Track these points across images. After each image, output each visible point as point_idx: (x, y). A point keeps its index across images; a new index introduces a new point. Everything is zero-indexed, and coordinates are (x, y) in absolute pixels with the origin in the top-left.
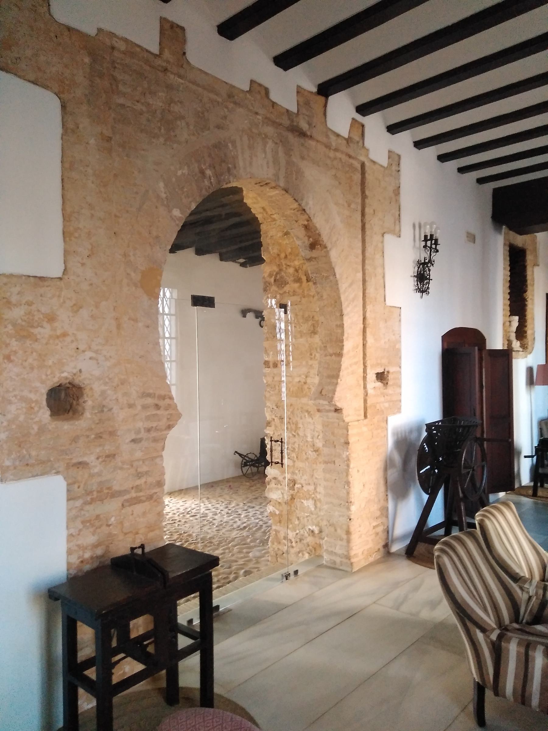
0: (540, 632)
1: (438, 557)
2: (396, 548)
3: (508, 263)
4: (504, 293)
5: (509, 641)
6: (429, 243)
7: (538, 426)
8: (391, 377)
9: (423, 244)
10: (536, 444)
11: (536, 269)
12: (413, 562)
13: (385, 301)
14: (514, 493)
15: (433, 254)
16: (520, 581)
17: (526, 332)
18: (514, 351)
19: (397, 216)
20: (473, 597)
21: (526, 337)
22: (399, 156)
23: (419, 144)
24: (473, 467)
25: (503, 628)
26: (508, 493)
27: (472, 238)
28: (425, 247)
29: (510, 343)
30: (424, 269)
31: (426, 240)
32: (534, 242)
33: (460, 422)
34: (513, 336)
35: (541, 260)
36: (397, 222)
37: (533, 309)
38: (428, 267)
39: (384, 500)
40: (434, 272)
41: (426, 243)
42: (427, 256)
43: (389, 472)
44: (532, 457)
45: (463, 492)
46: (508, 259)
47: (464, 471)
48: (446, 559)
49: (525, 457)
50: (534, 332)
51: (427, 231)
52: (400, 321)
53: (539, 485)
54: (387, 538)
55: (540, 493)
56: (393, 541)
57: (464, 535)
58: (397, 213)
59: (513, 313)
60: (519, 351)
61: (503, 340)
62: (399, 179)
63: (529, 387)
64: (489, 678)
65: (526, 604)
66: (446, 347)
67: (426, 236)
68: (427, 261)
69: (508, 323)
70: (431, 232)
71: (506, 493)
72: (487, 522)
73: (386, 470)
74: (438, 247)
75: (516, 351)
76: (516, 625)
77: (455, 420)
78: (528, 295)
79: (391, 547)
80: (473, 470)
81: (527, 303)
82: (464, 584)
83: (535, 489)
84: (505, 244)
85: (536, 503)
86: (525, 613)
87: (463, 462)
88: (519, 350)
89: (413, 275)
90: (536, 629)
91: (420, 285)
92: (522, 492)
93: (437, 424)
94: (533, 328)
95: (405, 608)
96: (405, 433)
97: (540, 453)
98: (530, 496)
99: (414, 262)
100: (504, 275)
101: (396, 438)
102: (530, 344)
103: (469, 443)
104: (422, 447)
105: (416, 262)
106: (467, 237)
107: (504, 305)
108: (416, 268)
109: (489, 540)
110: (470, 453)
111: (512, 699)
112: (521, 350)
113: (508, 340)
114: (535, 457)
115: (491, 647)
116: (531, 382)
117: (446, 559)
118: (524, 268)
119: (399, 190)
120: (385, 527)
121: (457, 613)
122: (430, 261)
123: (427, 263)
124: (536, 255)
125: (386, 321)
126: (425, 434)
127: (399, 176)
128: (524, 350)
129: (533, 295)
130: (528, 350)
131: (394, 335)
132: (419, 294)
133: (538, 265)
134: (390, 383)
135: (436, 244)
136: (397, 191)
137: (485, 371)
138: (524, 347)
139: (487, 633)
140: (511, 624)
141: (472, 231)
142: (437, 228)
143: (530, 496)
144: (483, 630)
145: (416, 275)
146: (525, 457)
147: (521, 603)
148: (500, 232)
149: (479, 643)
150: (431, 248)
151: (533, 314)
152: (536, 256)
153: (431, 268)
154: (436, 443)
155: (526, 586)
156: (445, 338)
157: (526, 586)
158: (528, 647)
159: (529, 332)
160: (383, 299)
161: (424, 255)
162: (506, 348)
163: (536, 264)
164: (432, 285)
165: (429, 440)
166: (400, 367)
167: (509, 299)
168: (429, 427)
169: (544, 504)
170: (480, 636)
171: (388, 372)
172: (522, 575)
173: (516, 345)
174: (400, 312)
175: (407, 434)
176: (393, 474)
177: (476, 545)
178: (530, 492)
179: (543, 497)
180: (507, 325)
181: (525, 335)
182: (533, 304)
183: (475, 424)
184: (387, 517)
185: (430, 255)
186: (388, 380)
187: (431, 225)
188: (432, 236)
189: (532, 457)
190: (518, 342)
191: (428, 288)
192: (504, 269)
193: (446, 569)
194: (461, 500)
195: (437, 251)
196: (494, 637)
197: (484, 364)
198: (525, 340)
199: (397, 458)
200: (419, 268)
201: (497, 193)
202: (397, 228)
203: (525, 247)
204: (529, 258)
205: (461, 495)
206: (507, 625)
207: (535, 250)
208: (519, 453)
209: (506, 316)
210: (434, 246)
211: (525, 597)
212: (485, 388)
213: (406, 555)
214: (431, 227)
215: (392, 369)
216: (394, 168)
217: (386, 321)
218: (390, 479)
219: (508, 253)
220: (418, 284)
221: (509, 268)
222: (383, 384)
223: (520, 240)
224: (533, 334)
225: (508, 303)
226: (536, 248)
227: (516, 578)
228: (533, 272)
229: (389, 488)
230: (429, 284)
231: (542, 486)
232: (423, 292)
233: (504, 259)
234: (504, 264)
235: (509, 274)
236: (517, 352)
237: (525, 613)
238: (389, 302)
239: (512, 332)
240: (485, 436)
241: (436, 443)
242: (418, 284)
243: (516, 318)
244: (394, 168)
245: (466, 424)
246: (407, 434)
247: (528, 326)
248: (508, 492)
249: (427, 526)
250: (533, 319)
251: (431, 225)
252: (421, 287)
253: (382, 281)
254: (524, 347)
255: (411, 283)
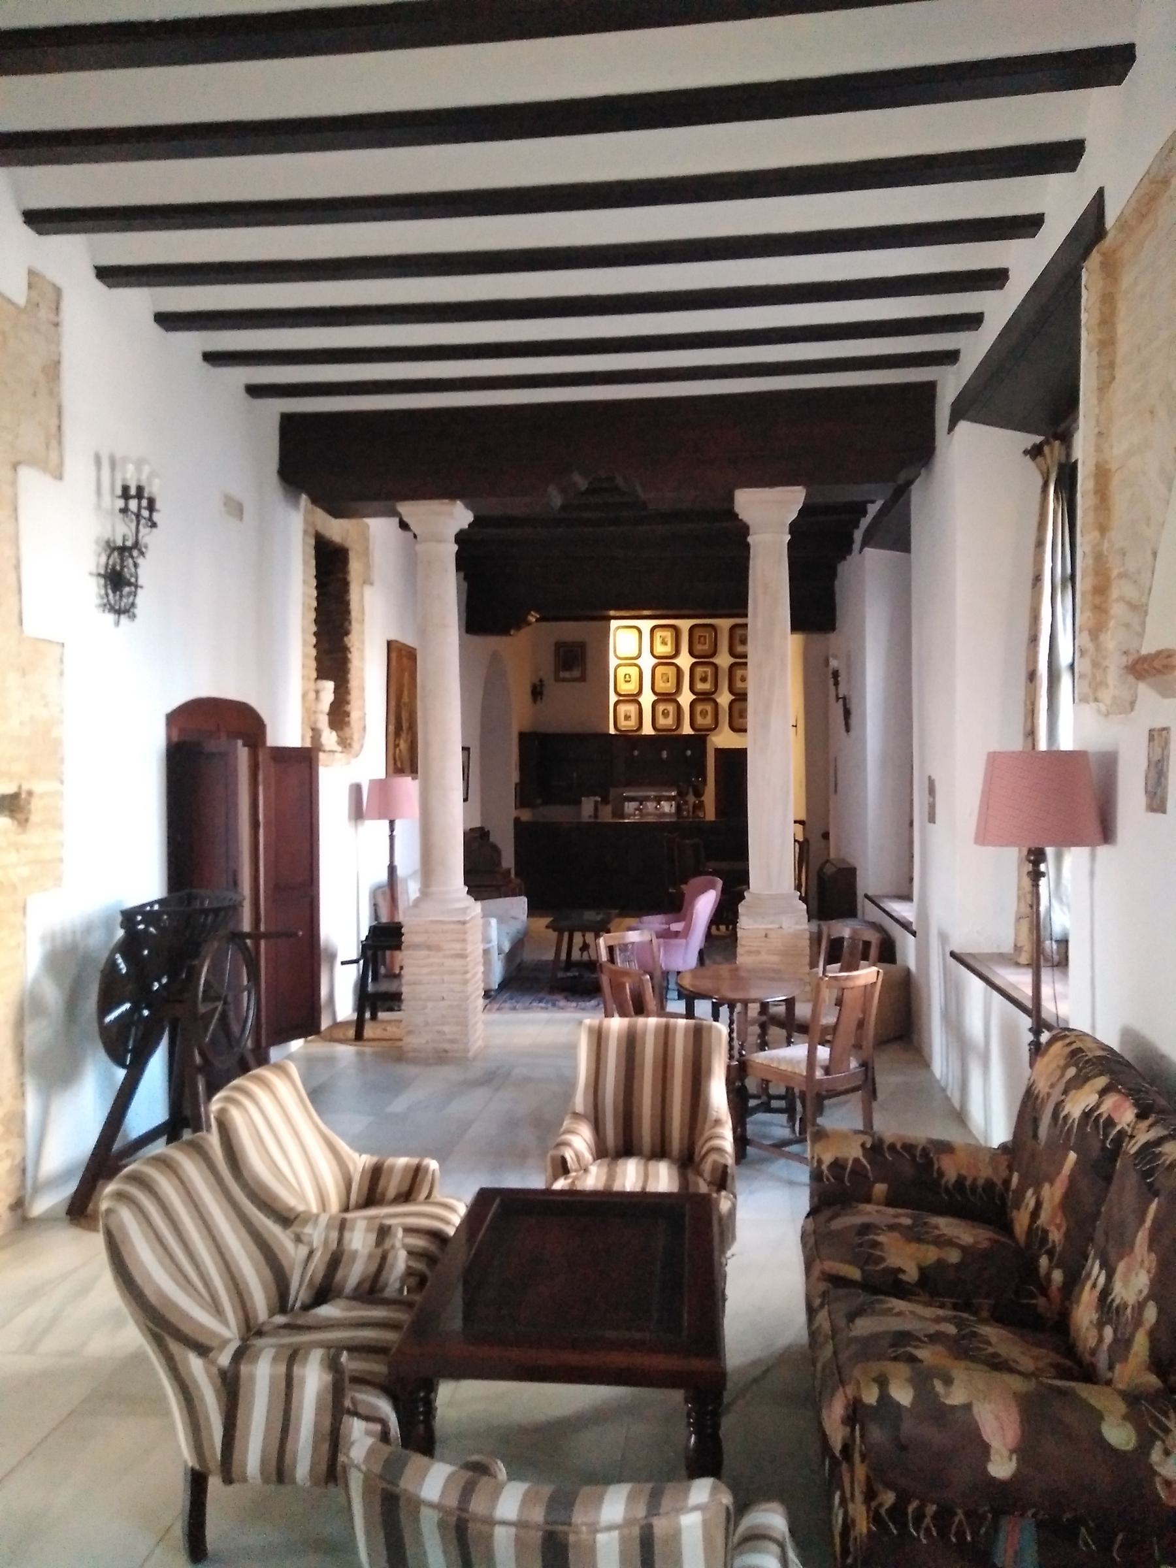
0: (329, 1319)
1: (109, 1211)
2: (45, 1204)
3: (313, 571)
4: (304, 631)
5: (255, 1359)
6: (133, 505)
7: (370, 900)
8: (36, 805)
9: (120, 503)
10: (364, 933)
11: (368, 592)
12: (84, 1228)
13: (21, 624)
14: (322, 1038)
15: (143, 530)
16: (296, 1223)
17: (348, 714)
18: (324, 751)
19: (54, 430)
20: (183, 1282)
21: (348, 724)
22: (58, 292)
23: (110, 275)
24: (226, 997)
25: (252, 1331)
26: (311, 1041)
27: (235, 508)
28: (125, 511)
29: (316, 734)
30: (122, 560)
31: (125, 494)
32: (365, 537)
33: (202, 903)
34: (323, 722)
35: (376, 575)
36: (54, 443)
37: (362, 670)
38: (132, 557)
39: (15, 1097)
40: (147, 571)
41: (126, 504)
42: (130, 535)
43: (30, 1029)
44: (356, 961)
45: (202, 1054)
46: (313, 562)
47: (202, 1009)
48: (126, 1215)
49: (343, 963)
50: (365, 714)
51: (128, 476)
52: (62, 674)
53: (368, 1015)
54: (22, 1186)
55: (369, 1031)
56: (37, 1189)
57: (181, 1149)
58: (54, 422)
59: (322, 674)
60: (333, 752)
61: (303, 729)
62: (58, 344)
63: (353, 822)
64: (213, 1446)
65: (302, 1269)
66: (175, 739)
67: (125, 489)
68: (129, 544)
69: (312, 695)
70: (139, 480)
71: (306, 1042)
72: (235, 1114)
73: (19, 1024)
74: (156, 517)
75: (329, 751)
76: (280, 1319)
77: (190, 898)
78: (353, 640)
79: (31, 1203)
80: (225, 1003)
81: (349, 656)
82: (167, 1261)
83: (360, 1024)
84: (305, 532)
85: (360, 1054)
86: (299, 1292)
87: (201, 988)
88: (334, 749)
89: (94, 571)
90: (316, 1315)
91: (114, 596)
92: (340, 1034)
93: (148, 908)
94: (362, 708)
95: (50, 1344)
96: (74, 933)
97: (369, 953)
98: (351, 1040)
99: (97, 542)
100: (304, 594)
101: (48, 946)
102: (356, 737)
103: (216, 944)
104: (112, 965)
105: (103, 544)
106: (225, 504)
107: (305, 656)
108: (103, 559)
109: (235, 1148)
110: (216, 969)
111: (259, 1480)
112: (339, 749)
113: (313, 729)
114: (361, 962)
115: (219, 1381)
116: (358, 813)
117: (126, 1215)
118: (345, 585)
119: (59, 372)
120: (18, 1159)
121: (150, 1330)
122: (136, 545)
123: (130, 549)
124: (368, 561)
125: (24, 674)
126: (120, 933)
127: (59, 335)
128: (344, 750)
129: (363, 643)
130: (353, 751)
131: (46, 705)
132: (110, 617)
133: (372, 584)
134: (35, 818)
135: (151, 507)
136: (53, 370)
137: (264, 790)
138: (345, 743)
139: (211, 1355)
140: (270, 1320)
141: (237, 492)
142: (153, 474)
143: (351, 1040)
144: (203, 1350)
145: (102, 572)
146: (343, 963)
147: (292, 1268)
148: (296, 503)
149: (195, 1381)
150: (138, 516)
151: (362, 679)
152: (368, 566)
153: (140, 561)
154: (146, 952)
155: (308, 1230)
156: (174, 718)
157: (308, 1230)
158: (293, 1357)
159: (355, 715)
160: (15, 620)
161: (122, 531)
162: (308, 744)
163: (367, 581)
164: (144, 600)
165: (130, 945)
166: (62, 782)
167: (315, 646)
168: (129, 917)
169: (375, 1054)
170: (195, 1365)
171: (30, 794)
172: (301, 1208)
173: (329, 738)
174: (62, 654)
175: (79, 936)
176: (40, 1033)
177: (204, 1166)
178: (351, 1033)
179: (374, 1040)
180: (310, 699)
181: (347, 719)
182: (362, 659)
183: (231, 903)
184: (22, 1135)
185: (137, 531)
186: (29, 811)
187: (139, 463)
188: (140, 489)
189: (356, 961)
190: (334, 733)
191: (133, 605)
192: (305, 582)
193: (126, 1235)
194: (200, 1069)
195: (154, 525)
196: (224, 1359)
197: (261, 777)
198: (347, 729)
199: (52, 995)
200: (109, 557)
201: (289, 422)
202: (54, 456)
203: (347, 545)
204: (355, 567)
205: (198, 1059)
206: (263, 1324)
207: (366, 553)
208: (332, 957)
209: (309, 679)
210: (145, 513)
211: (303, 1251)
212: (265, 827)
213: (68, 1217)
214: (139, 469)
215: (39, 787)
216: (44, 313)
217: (24, 674)
218: (30, 1047)
219: (313, 552)
220: (107, 595)
221: (314, 583)
222: (16, 823)
223: (337, 529)
224: (363, 718)
225: (314, 652)
226: (367, 548)
227: (286, 1219)
228: (362, 597)
229: (27, 1066)
230: (135, 596)
231: (374, 1017)
232: (119, 612)
233: (305, 563)
234: (304, 571)
235: (315, 593)
236: (331, 753)
237: (299, 1292)
238: (32, 628)
239: (321, 712)
240: (262, 928)
241: (146, 952)
242: (107, 595)
243: (329, 685)
244: (44, 313)
245: (216, 905)
246: (79, 936)
247: (352, 703)
248: (310, 1038)
249: (126, 1136)
250: (362, 689)
251: (139, 463)
252: (115, 601)
253: (12, 577)
254: (345, 743)
255: (92, 589)
